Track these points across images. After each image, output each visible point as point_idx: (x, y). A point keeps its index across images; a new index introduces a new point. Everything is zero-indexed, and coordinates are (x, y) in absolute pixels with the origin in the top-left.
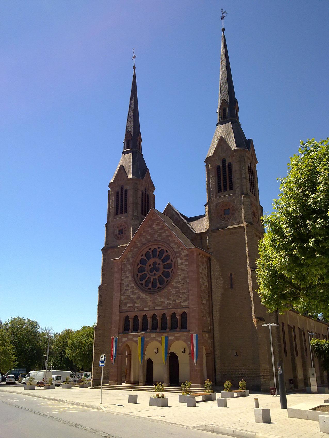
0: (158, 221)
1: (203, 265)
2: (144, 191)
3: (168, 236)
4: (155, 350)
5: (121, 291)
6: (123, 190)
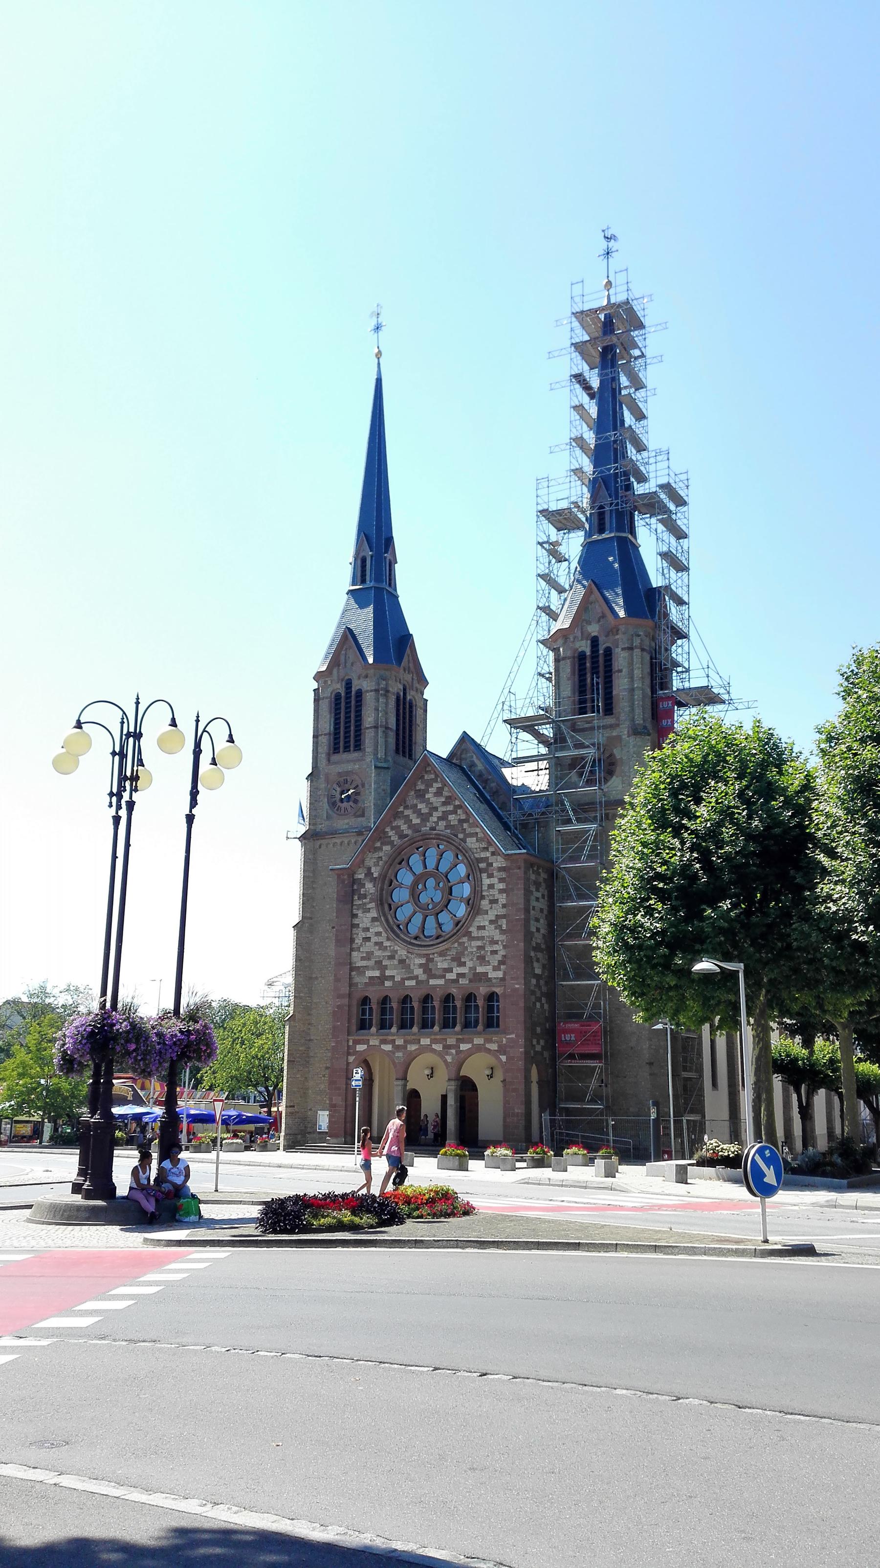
0: (440, 785)
1: (537, 890)
2: (402, 694)
3: (461, 821)
4: (427, 1072)
5: (352, 940)
6: (351, 692)
